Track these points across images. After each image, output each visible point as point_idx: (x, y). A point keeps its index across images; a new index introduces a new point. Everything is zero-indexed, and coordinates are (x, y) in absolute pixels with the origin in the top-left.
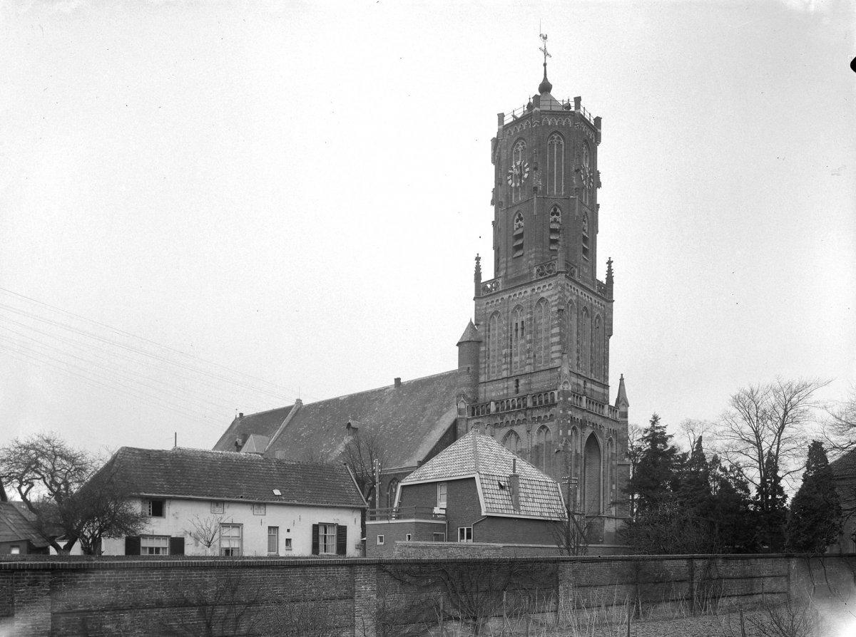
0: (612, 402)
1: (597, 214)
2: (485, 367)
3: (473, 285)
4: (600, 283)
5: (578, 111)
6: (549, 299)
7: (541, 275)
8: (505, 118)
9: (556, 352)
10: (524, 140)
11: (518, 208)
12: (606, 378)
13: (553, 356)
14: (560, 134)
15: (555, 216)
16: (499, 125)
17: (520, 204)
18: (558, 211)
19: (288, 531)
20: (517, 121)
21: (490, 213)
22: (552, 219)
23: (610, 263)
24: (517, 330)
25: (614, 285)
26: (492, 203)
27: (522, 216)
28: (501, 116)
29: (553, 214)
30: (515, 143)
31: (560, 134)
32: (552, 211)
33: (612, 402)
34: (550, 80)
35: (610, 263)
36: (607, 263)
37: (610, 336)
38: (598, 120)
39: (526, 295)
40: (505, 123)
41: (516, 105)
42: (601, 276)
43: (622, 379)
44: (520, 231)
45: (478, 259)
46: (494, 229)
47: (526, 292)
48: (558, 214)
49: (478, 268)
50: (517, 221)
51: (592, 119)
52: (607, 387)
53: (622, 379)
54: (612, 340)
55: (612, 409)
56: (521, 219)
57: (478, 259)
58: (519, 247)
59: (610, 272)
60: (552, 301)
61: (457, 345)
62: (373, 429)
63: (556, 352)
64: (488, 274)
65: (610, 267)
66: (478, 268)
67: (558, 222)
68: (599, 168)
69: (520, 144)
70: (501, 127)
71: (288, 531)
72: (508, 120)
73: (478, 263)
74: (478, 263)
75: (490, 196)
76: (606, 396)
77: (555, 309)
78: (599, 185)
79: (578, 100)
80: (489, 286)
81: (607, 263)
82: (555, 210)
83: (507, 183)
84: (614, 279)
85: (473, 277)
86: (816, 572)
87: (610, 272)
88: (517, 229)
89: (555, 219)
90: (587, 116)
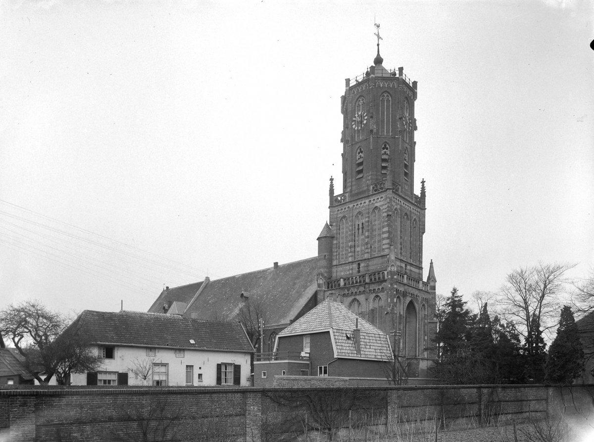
0: (425, 279)
1: (414, 148)
2: (337, 255)
3: (328, 198)
4: (416, 197)
5: (401, 77)
6: (381, 208)
7: (376, 191)
8: (350, 82)
9: (386, 244)
10: (364, 97)
11: (359, 144)
12: (421, 262)
13: (384, 247)
14: (389, 93)
15: (385, 150)
16: (346, 87)
17: (361, 141)
18: (387, 146)
19: (200, 368)
20: (359, 84)
21: (340, 148)
22: (383, 152)
23: (423, 182)
24: (359, 229)
25: (426, 198)
26: (342, 141)
27: (362, 150)
28: (348, 81)
29: (383, 149)
30: (357, 99)
31: (389, 93)
32: (383, 146)
33: (425, 279)
34: (382, 55)
35: (423, 182)
36: (421, 183)
37: (423, 233)
38: (415, 83)
39: (365, 204)
40: (351, 85)
41: (358, 73)
42: (417, 191)
43: (431, 263)
44: (361, 160)
45: (332, 180)
46: (343, 159)
47: (365, 203)
48: (387, 149)
49: (332, 186)
50: (359, 154)
51: (411, 83)
52: (421, 268)
53: (431, 263)
54: (424, 236)
55: (425, 284)
56: (362, 152)
57: (332, 180)
58: (360, 172)
59: (423, 189)
60: (383, 209)
61: (317, 239)
62: (259, 298)
63: (386, 244)
64: (339, 190)
65: (423, 185)
66: (332, 186)
67: (387, 154)
68: (416, 116)
69: (361, 100)
70: (348, 88)
71: (200, 368)
72: (353, 83)
73: (332, 182)
74: (332, 182)
75: (340, 136)
76: (421, 275)
77: (385, 214)
78: (416, 128)
79: (401, 69)
80: (339, 198)
81: (421, 183)
82: (385, 146)
83: (352, 127)
84: (426, 194)
85: (328, 193)
86: (566, 397)
87: (423, 189)
88: (359, 159)
89: (385, 152)
90: (407, 81)
